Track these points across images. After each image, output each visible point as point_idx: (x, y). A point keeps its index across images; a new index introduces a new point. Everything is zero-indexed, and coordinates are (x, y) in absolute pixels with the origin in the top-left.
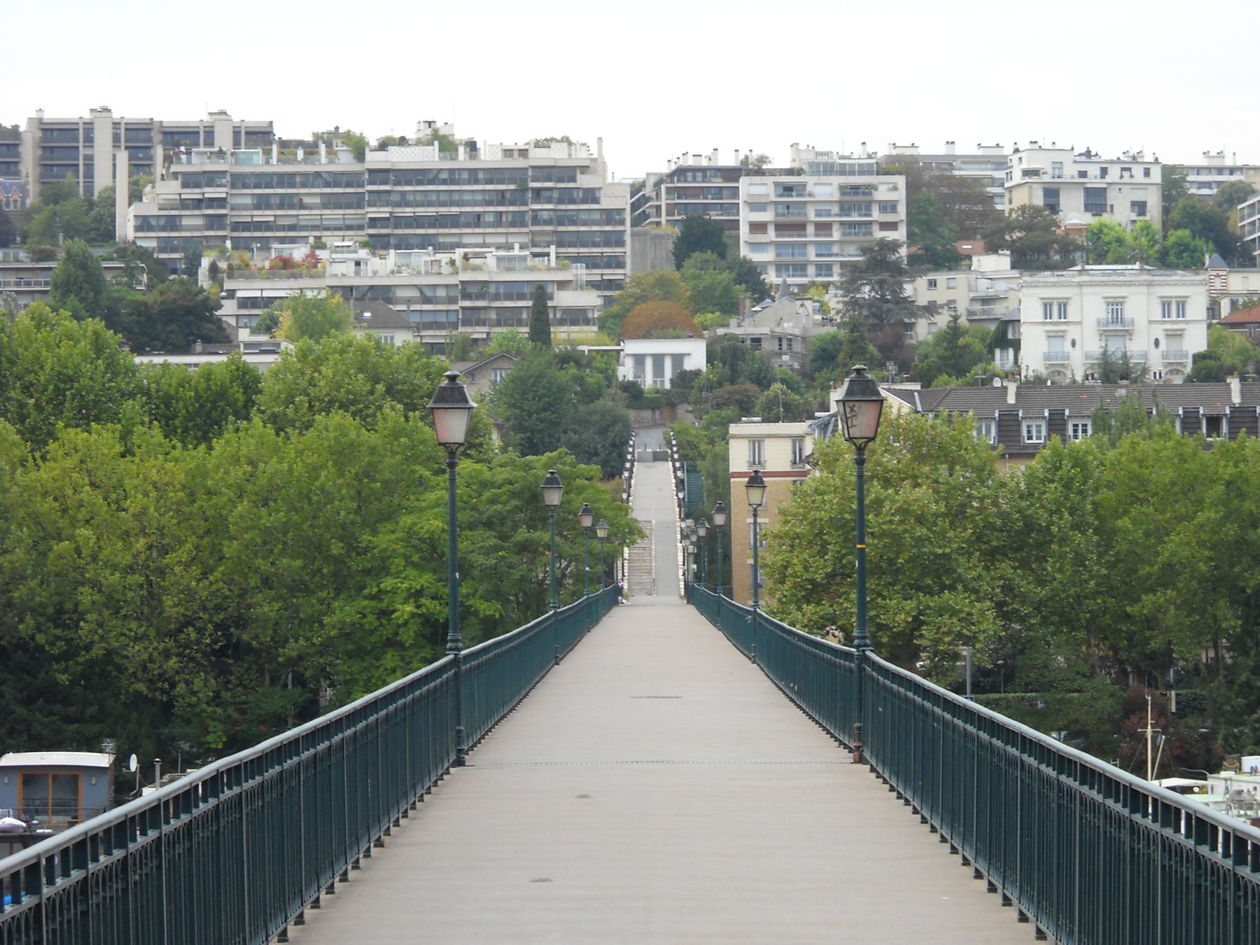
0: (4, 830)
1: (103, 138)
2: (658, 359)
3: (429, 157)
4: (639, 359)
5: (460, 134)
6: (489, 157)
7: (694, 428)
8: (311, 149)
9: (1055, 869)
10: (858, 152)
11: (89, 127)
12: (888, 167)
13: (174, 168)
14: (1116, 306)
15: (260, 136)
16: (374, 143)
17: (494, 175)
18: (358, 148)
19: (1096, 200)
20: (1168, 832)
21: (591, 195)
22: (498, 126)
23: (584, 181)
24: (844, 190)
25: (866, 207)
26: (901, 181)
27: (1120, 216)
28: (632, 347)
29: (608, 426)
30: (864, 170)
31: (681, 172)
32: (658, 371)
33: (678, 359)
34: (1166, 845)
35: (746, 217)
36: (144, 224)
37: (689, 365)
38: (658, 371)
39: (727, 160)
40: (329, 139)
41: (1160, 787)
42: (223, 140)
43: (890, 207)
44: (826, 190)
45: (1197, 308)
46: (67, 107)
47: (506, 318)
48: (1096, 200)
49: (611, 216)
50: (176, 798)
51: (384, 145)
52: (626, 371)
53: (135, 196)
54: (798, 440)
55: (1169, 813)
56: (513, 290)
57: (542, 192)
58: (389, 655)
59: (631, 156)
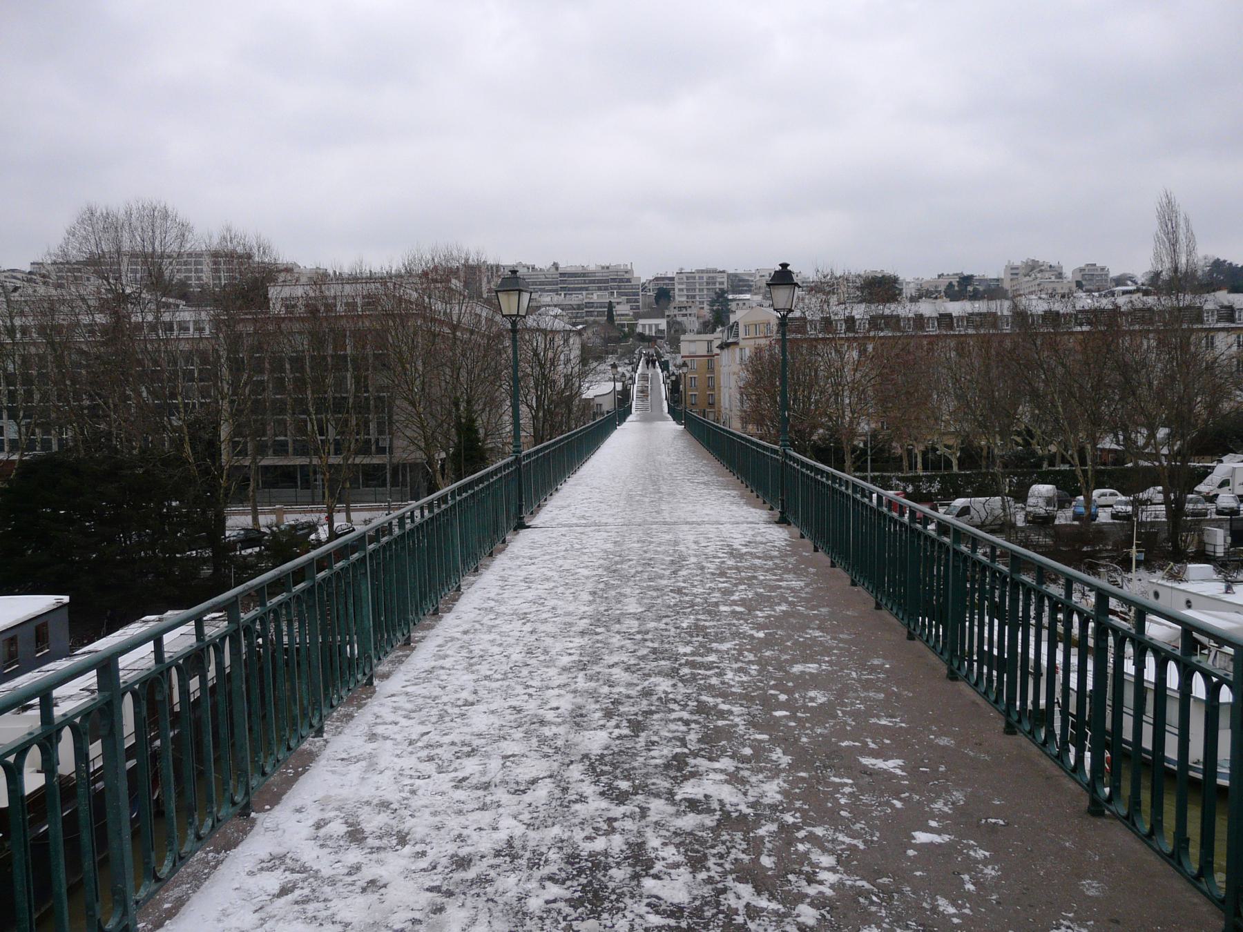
2: (650, 326)
4: (644, 326)
9: (1110, 682)
13: (125, 259)
16: (909, 291)
25: (714, 283)
28: (641, 322)
31: (657, 279)
32: (650, 329)
33: (657, 326)
35: (677, 287)
37: (661, 328)
38: (650, 329)
47: (600, 314)
50: (294, 573)
52: (639, 329)
56: (601, 305)
57: (617, 280)
58: (1108, 439)
59: (644, 273)
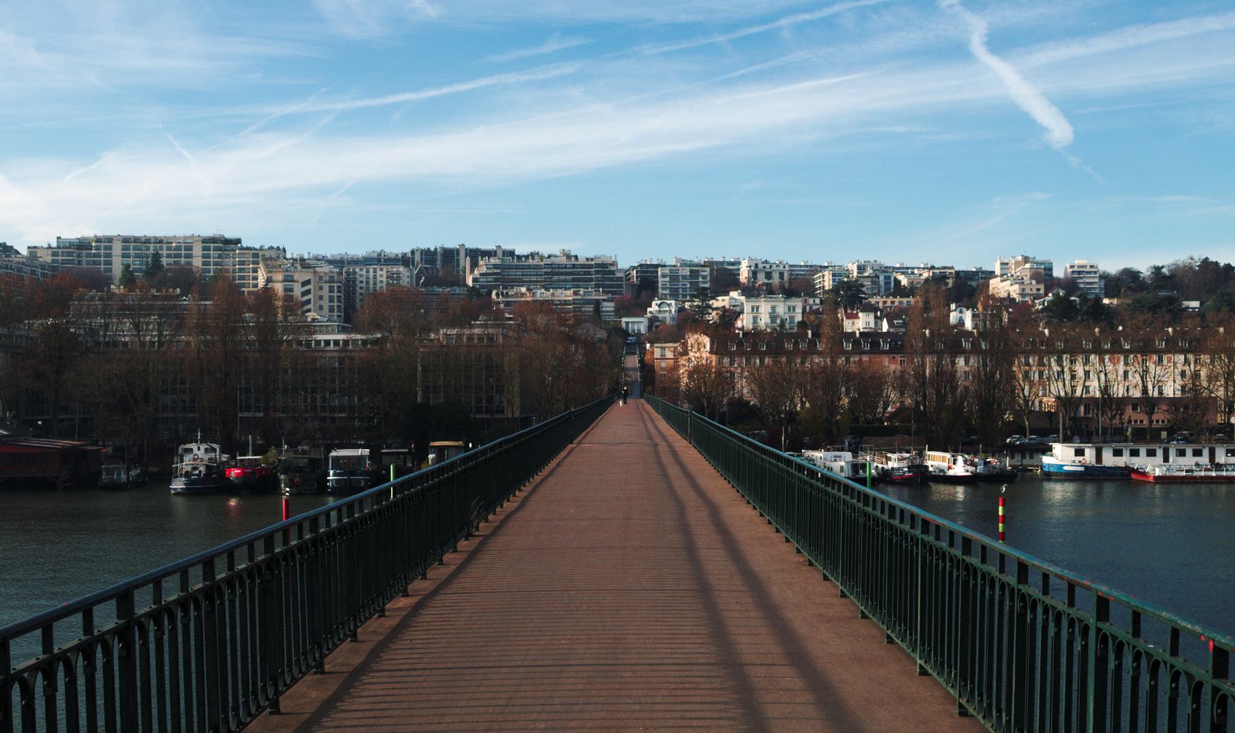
0: (107, 730)
1: (462, 254)
3: (564, 260)
5: (573, 253)
6: (582, 261)
7: (886, 406)
8: (527, 257)
10: (696, 261)
11: (458, 251)
12: (709, 264)
14: (773, 308)
15: (511, 253)
17: (583, 266)
18: (542, 258)
19: (769, 275)
20: (800, 475)
21: (613, 273)
22: (586, 249)
23: (612, 268)
24: (691, 271)
25: (697, 277)
26: (708, 269)
27: (776, 280)
28: (624, 320)
29: (514, 281)
30: (698, 265)
31: (641, 265)
34: (799, 478)
36: (475, 280)
39: (655, 262)
40: (532, 255)
41: (786, 455)
42: (500, 254)
43: (704, 277)
44: (686, 271)
45: (799, 310)
46: (451, 244)
48: (769, 275)
49: (620, 279)
51: (549, 256)
53: (472, 271)
54: (675, 348)
55: (789, 463)
